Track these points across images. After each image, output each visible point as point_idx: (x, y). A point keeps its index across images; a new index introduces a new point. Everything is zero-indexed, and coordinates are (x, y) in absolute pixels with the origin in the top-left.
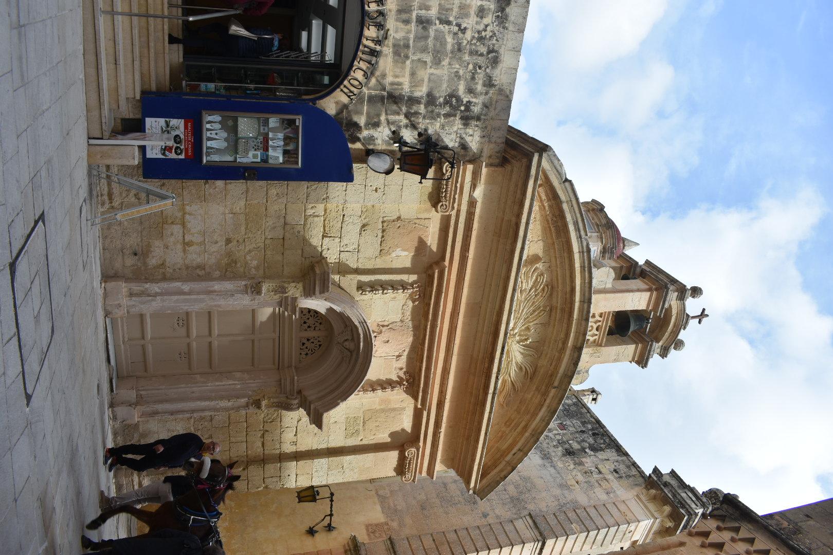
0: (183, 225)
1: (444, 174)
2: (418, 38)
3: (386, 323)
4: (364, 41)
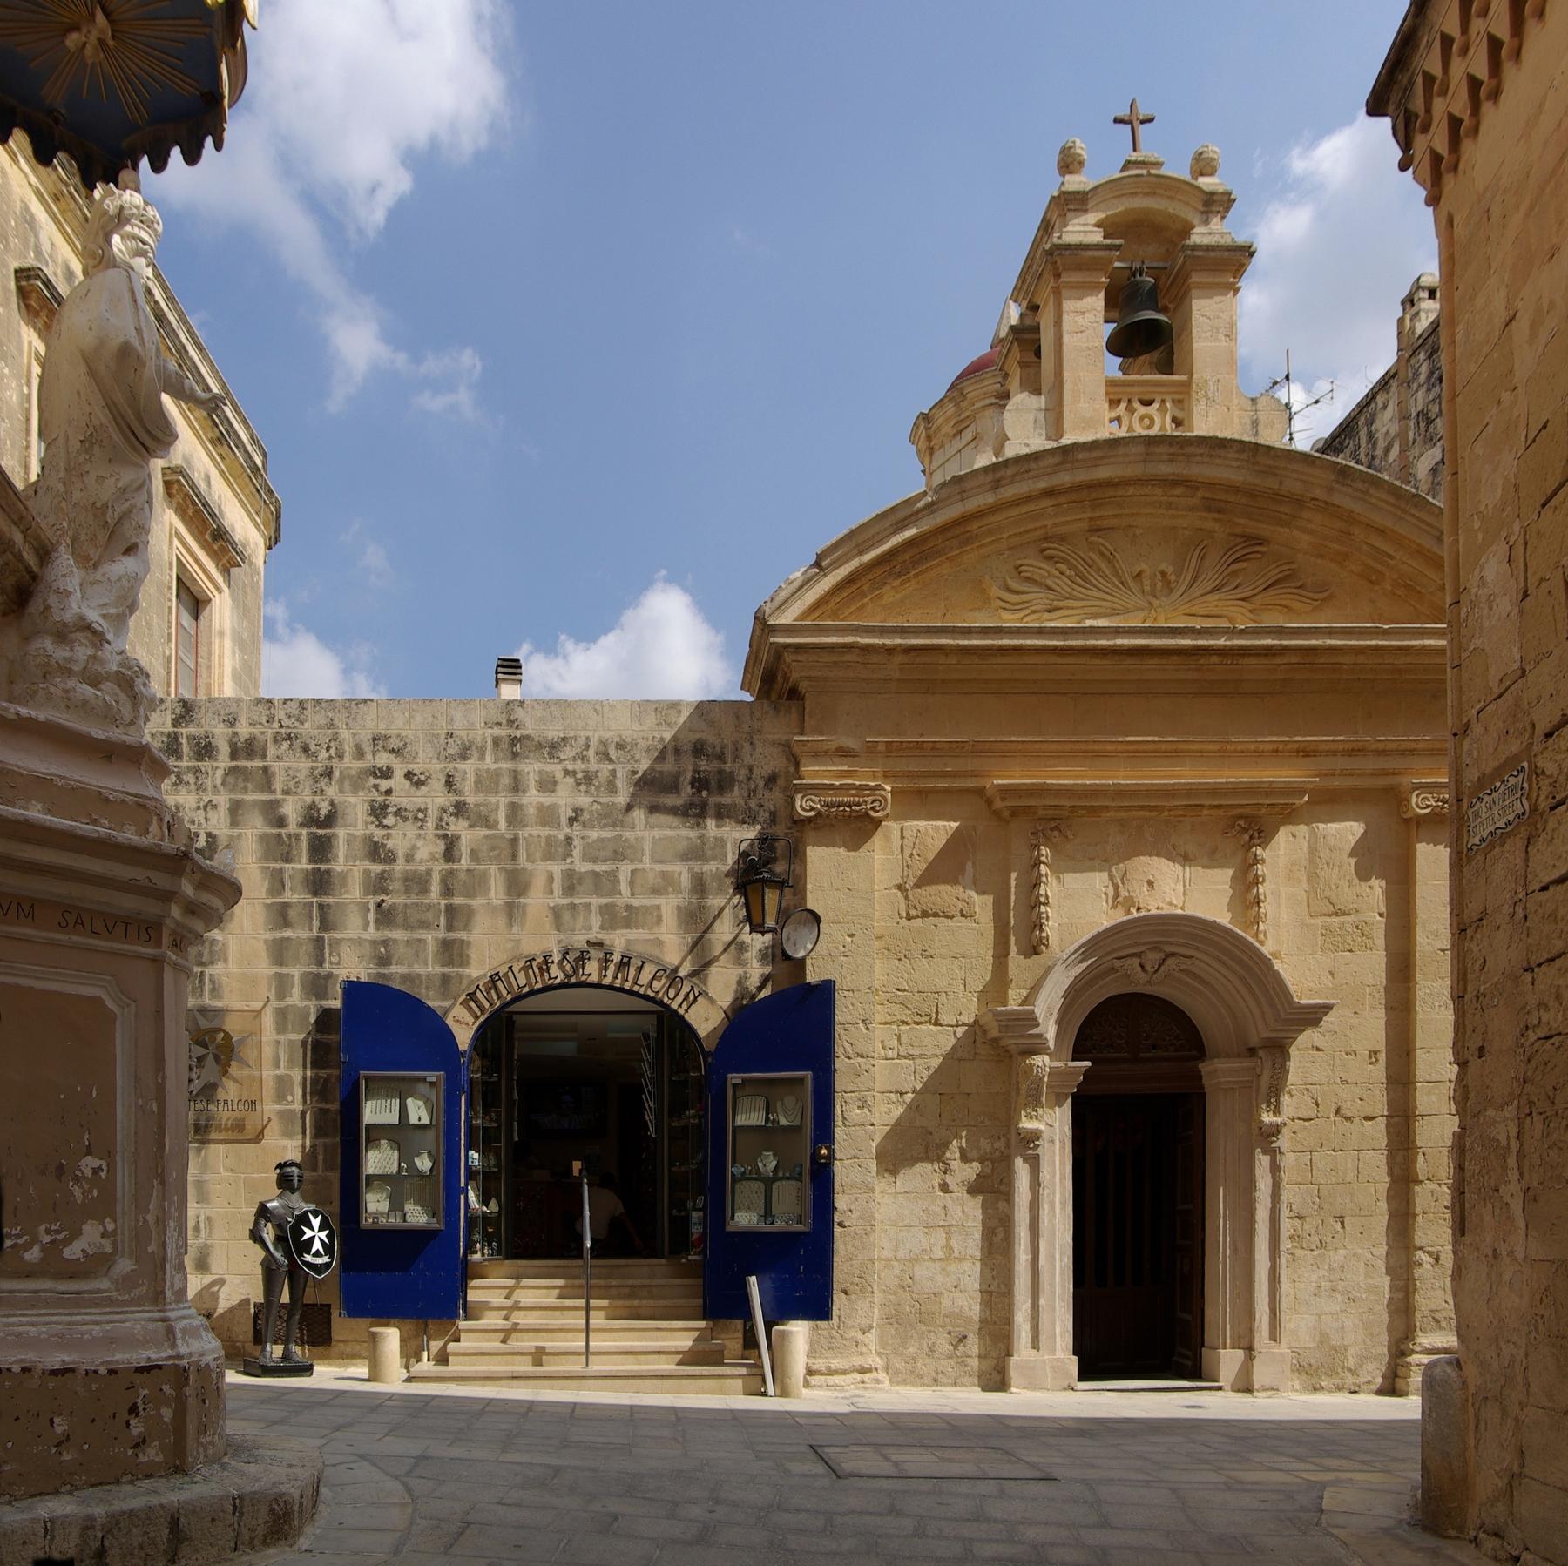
0: (914, 1261)
1: (819, 814)
2: (597, 891)
3: (1111, 891)
4: (607, 981)
